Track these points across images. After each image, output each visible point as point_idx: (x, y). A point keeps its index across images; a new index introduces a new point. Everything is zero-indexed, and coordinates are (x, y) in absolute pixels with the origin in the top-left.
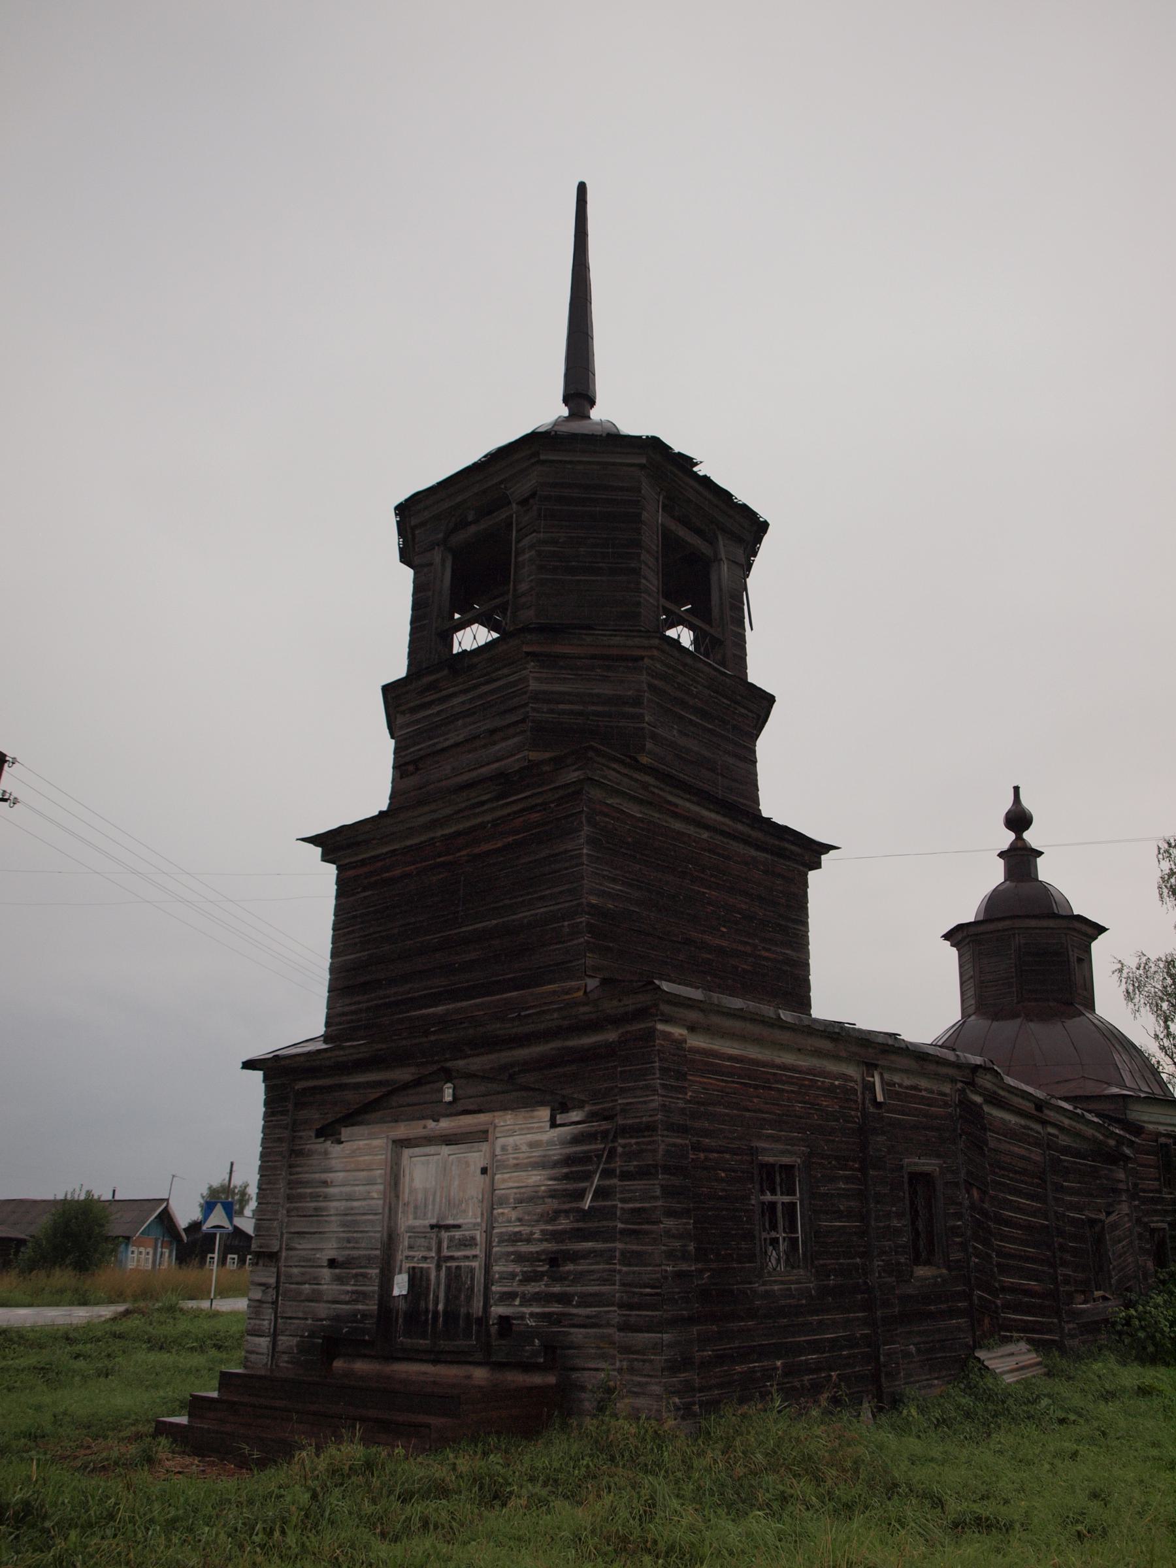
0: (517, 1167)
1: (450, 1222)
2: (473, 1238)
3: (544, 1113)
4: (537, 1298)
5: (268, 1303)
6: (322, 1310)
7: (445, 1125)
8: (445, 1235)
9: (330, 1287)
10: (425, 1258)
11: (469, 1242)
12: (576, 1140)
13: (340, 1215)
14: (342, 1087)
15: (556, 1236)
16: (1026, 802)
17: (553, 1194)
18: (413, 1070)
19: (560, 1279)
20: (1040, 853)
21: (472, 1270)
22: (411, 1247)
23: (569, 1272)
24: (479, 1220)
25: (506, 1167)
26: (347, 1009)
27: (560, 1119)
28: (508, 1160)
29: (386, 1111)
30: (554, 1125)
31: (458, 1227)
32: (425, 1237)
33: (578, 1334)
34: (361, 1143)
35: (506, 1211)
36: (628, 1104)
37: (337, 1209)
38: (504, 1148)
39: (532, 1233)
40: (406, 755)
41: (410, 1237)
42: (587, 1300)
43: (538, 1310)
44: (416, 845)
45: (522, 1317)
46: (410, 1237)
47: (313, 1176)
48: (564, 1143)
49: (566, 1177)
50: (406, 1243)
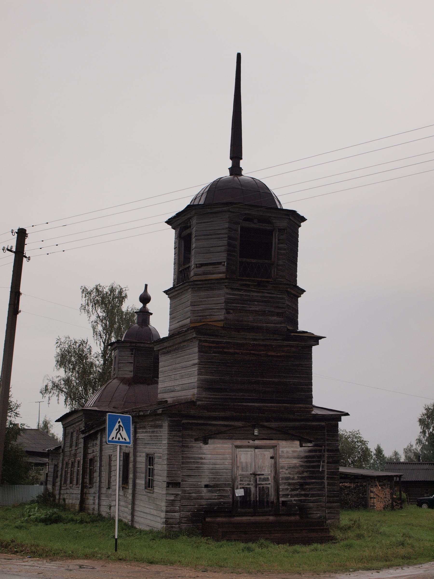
0: (288, 457)
1: (259, 473)
2: (268, 478)
3: (298, 443)
4: (297, 495)
5: (178, 500)
6: (203, 502)
7: (257, 442)
8: (258, 477)
9: (206, 494)
10: (249, 484)
11: (267, 479)
12: (310, 451)
13: (209, 470)
14: (207, 425)
15: (302, 478)
16: (149, 292)
17: (301, 466)
18: (243, 423)
19: (304, 490)
20: (151, 314)
21: (268, 488)
22: (241, 481)
23: (307, 488)
24: (270, 473)
25: (283, 457)
26: (208, 396)
27: (304, 445)
28: (284, 455)
29: (225, 435)
30: (301, 446)
31: (263, 474)
32: (248, 478)
33: (311, 505)
34: (218, 445)
35: (284, 470)
36: (329, 443)
37: (208, 467)
38: (282, 452)
39: (294, 477)
40: (231, 306)
41: (240, 478)
42: (313, 496)
43: (296, 499)
44: (241, 343)
45: (291, 501)
46: (240, 478)
47: (195, 455)
48: (305, 452)
49: (306, 462)
50: (239, 479)
